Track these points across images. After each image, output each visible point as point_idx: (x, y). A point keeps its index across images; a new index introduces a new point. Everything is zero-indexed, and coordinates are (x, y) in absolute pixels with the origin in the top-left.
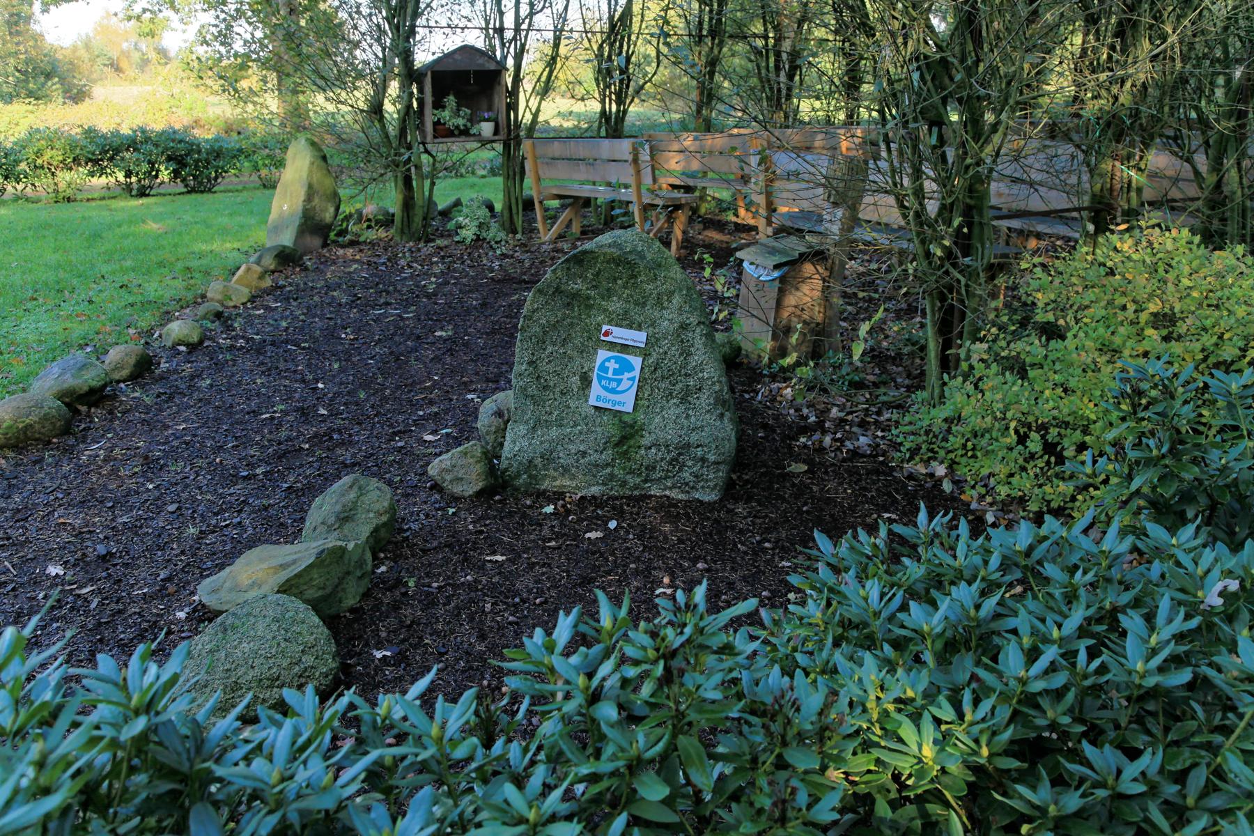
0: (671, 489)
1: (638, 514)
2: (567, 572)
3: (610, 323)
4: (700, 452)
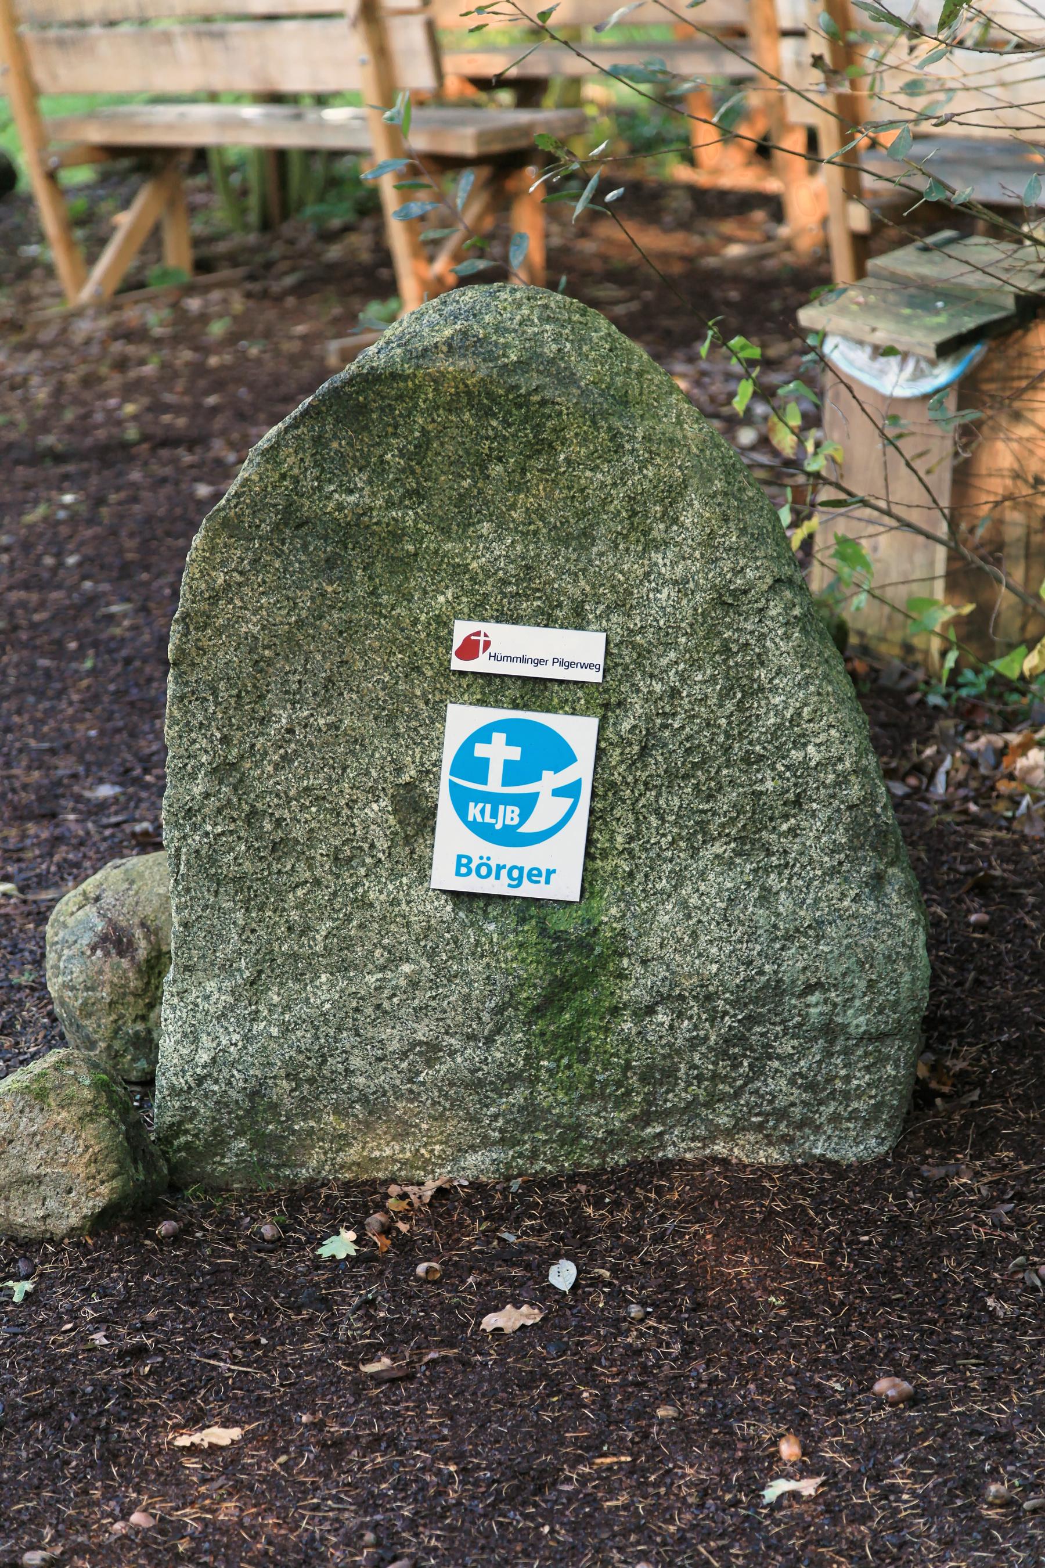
0: (729, 1134)
1: (635, 1229)
2: (458, 1457)
3: (476, 612)
4: (816, 1007)
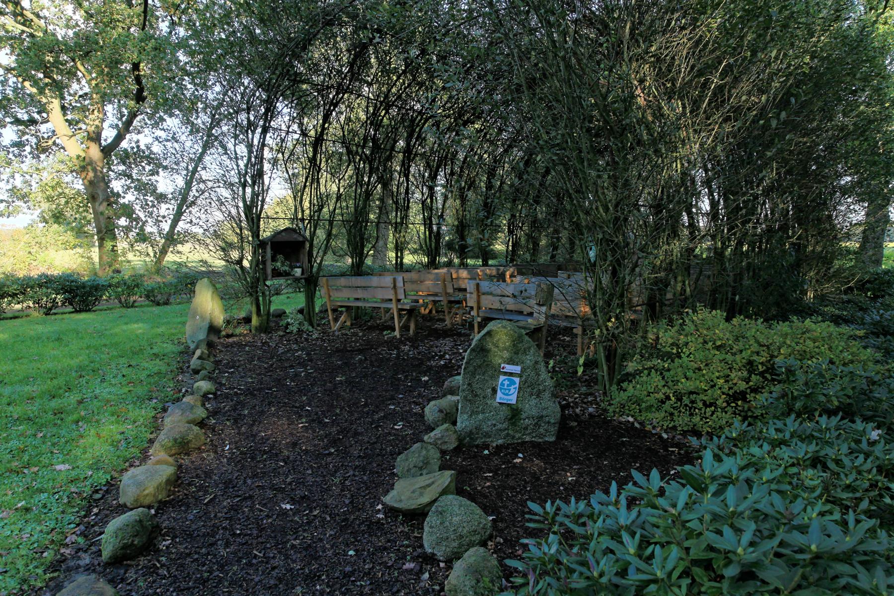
4: (547, 419)
